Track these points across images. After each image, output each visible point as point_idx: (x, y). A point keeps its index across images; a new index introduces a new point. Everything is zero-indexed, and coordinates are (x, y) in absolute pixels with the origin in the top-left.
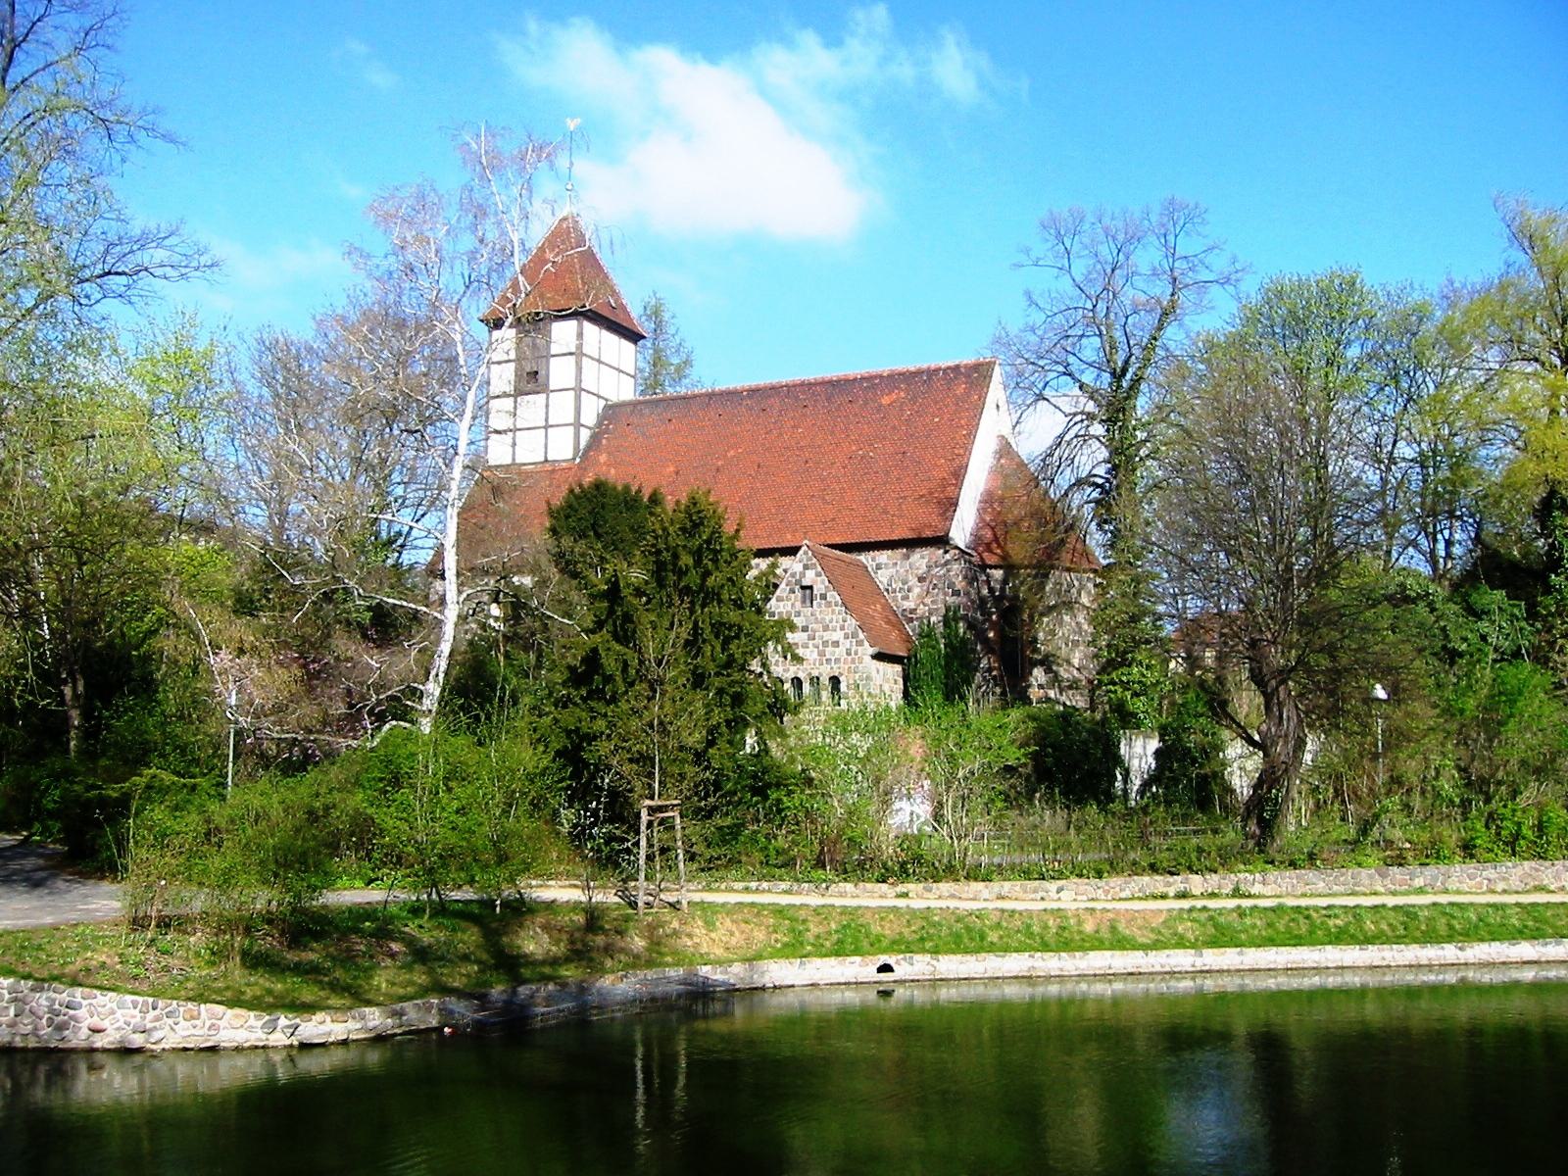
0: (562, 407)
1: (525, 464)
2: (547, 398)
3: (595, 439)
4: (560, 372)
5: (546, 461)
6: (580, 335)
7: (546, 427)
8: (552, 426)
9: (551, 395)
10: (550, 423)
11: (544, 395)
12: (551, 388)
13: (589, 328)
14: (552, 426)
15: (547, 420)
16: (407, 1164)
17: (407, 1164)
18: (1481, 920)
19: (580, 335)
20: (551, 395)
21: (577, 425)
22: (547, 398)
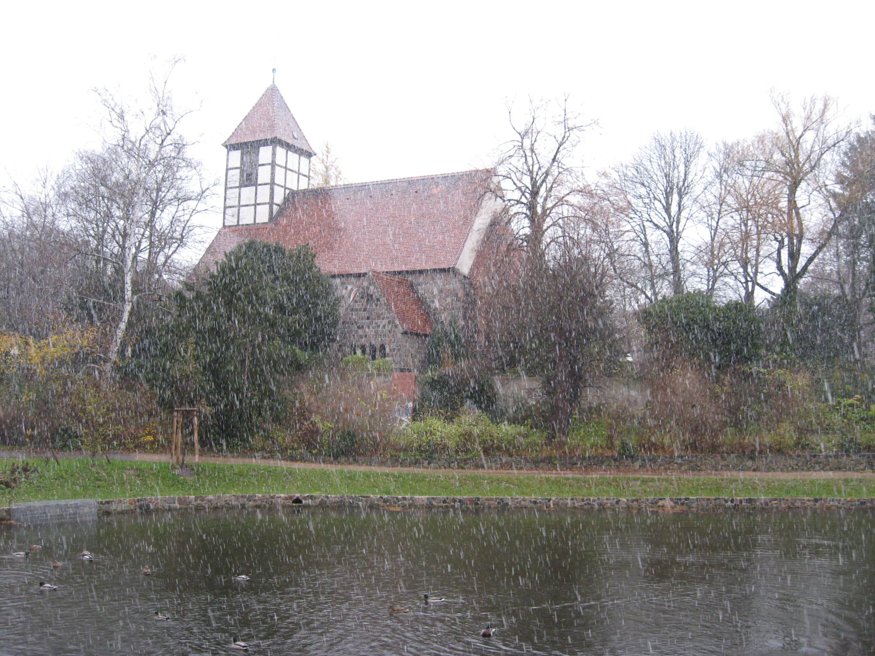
0: (264, 194)
1: (662, 204)
2: (256, 189)
3: (281, 213)
4: (264, 174)
5: (238, 225)
6: (274, 154)
7: (240, 206)
8: (259, 204)
9: (259, 187)
10: (258, 202)
11: (254, 188)
12: (259, 182)
13: (280, 151)
14: (259, 204)
15: (239, 203)
16: (4, 613)
17: (4, 613)
18: (595, 319)
19: (274, 154)
20: (259, 187)
21: (271, 203)
22: (256, 189)
